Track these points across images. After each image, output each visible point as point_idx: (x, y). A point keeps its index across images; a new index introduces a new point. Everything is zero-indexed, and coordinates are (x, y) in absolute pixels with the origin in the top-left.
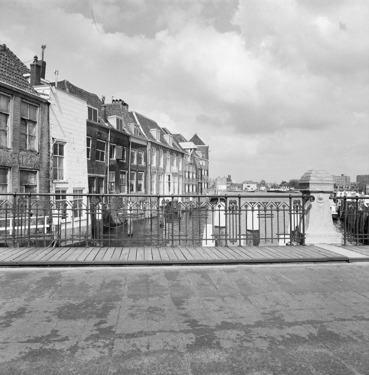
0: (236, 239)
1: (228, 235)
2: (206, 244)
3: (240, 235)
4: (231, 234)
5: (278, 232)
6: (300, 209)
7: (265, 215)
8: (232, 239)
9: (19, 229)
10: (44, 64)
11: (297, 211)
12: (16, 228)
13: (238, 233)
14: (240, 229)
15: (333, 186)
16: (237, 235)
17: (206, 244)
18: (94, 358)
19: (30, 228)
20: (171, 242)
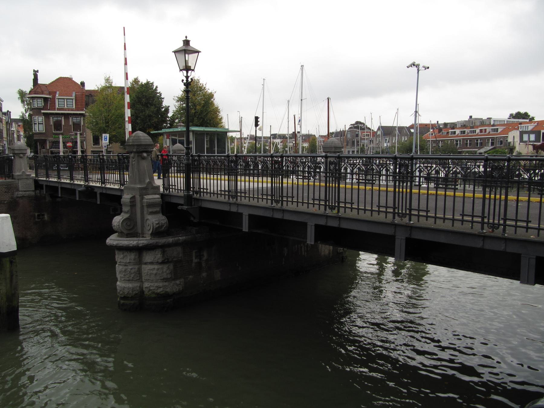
0: (499, 225)
1: (486, 217)
2: (217, 198)
3: (505, 220)
4: (179, 185)
5: (314, 197)
6: (420, 174)
7: (365, 180)
8: (491, 224)
9: (497, 198)
10: (94, 385)
11: (332, 174)
12: (362, 187)
13: (502, 216)
14: (507, 210)
15: (299, 131)
16: (487, 217)
17: (217, 198)
18: (374, 279)
19: (519, 199)
20: (408, 217)
